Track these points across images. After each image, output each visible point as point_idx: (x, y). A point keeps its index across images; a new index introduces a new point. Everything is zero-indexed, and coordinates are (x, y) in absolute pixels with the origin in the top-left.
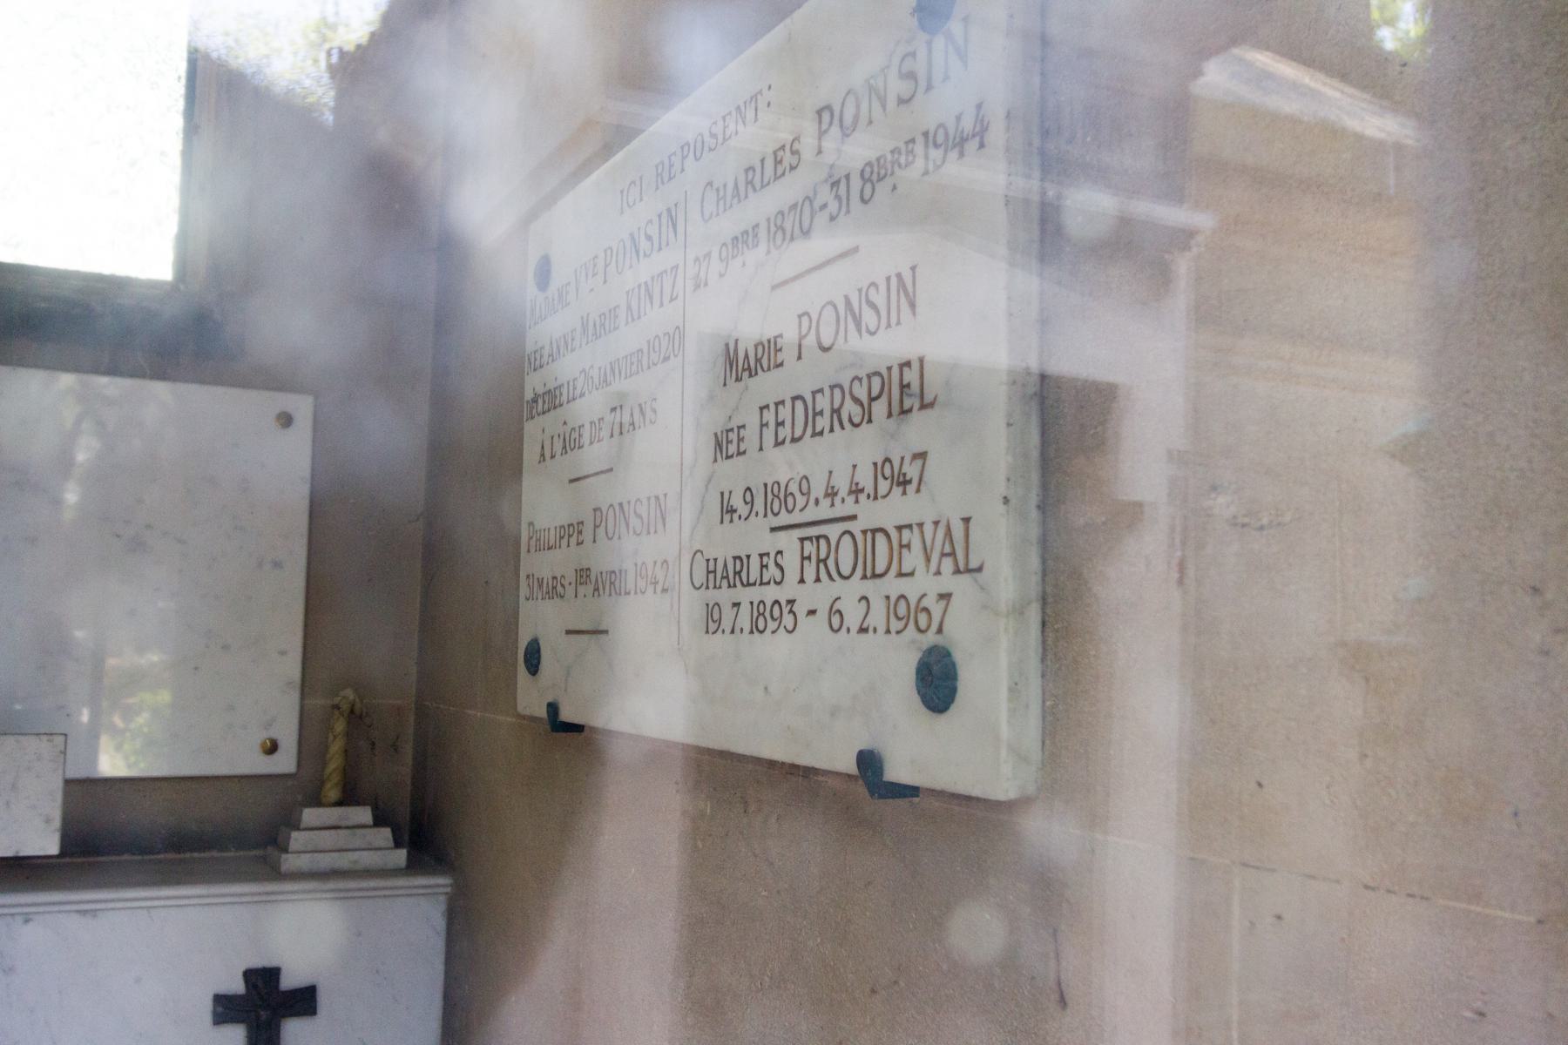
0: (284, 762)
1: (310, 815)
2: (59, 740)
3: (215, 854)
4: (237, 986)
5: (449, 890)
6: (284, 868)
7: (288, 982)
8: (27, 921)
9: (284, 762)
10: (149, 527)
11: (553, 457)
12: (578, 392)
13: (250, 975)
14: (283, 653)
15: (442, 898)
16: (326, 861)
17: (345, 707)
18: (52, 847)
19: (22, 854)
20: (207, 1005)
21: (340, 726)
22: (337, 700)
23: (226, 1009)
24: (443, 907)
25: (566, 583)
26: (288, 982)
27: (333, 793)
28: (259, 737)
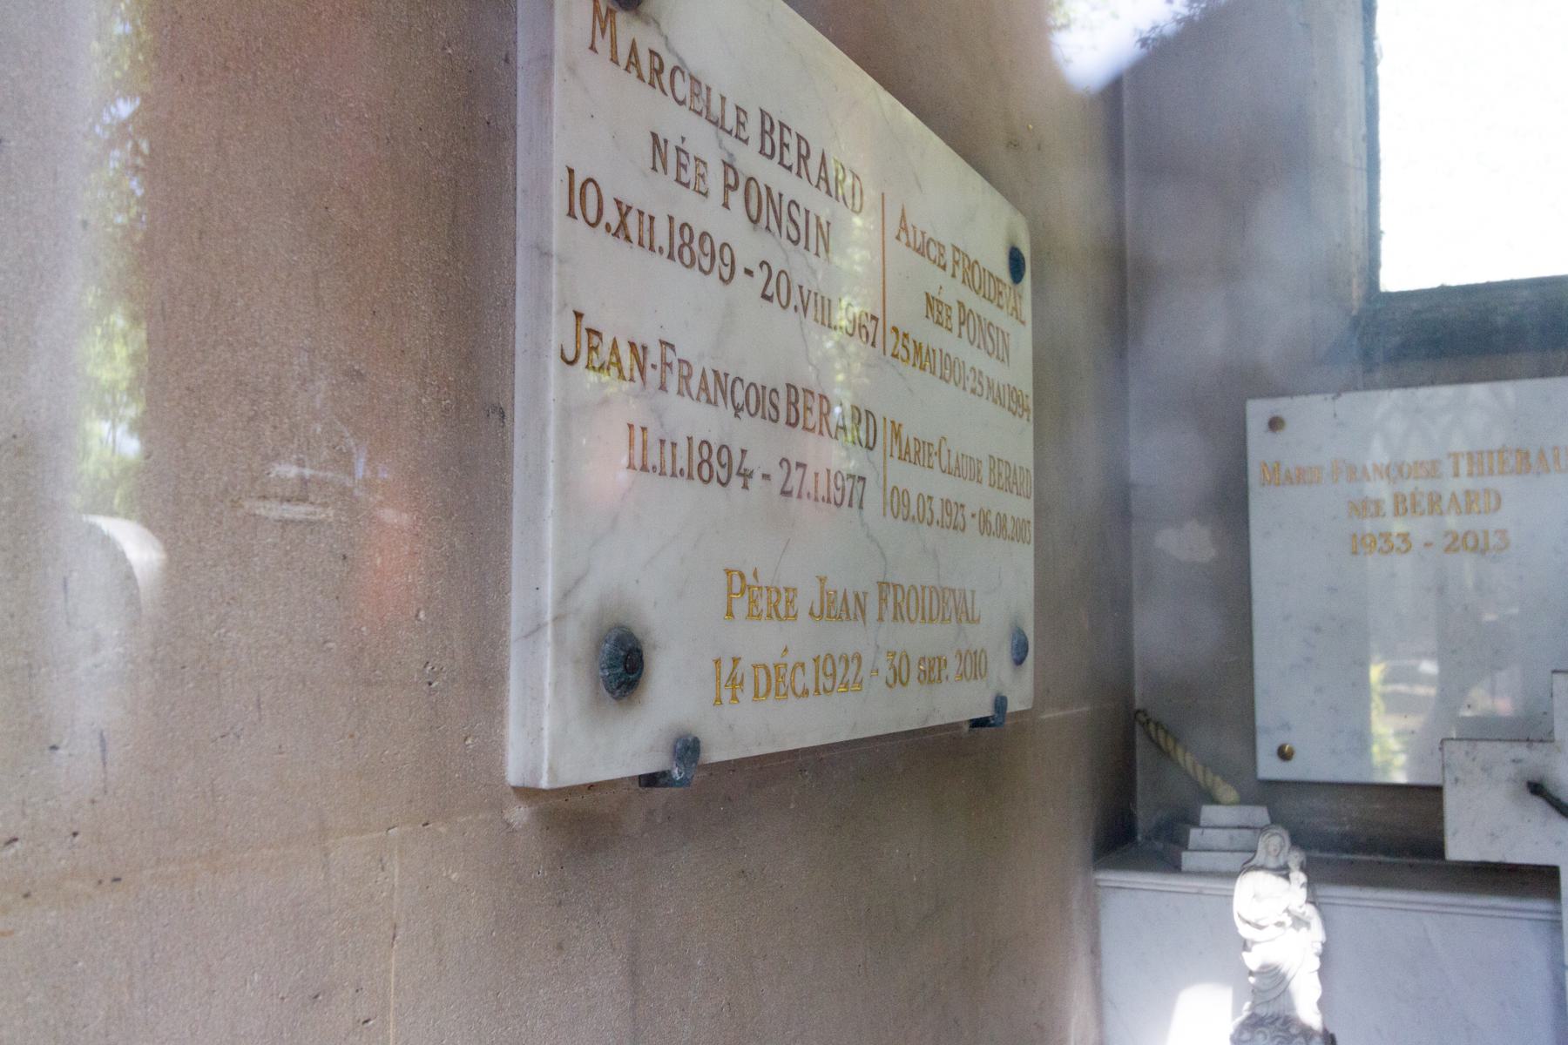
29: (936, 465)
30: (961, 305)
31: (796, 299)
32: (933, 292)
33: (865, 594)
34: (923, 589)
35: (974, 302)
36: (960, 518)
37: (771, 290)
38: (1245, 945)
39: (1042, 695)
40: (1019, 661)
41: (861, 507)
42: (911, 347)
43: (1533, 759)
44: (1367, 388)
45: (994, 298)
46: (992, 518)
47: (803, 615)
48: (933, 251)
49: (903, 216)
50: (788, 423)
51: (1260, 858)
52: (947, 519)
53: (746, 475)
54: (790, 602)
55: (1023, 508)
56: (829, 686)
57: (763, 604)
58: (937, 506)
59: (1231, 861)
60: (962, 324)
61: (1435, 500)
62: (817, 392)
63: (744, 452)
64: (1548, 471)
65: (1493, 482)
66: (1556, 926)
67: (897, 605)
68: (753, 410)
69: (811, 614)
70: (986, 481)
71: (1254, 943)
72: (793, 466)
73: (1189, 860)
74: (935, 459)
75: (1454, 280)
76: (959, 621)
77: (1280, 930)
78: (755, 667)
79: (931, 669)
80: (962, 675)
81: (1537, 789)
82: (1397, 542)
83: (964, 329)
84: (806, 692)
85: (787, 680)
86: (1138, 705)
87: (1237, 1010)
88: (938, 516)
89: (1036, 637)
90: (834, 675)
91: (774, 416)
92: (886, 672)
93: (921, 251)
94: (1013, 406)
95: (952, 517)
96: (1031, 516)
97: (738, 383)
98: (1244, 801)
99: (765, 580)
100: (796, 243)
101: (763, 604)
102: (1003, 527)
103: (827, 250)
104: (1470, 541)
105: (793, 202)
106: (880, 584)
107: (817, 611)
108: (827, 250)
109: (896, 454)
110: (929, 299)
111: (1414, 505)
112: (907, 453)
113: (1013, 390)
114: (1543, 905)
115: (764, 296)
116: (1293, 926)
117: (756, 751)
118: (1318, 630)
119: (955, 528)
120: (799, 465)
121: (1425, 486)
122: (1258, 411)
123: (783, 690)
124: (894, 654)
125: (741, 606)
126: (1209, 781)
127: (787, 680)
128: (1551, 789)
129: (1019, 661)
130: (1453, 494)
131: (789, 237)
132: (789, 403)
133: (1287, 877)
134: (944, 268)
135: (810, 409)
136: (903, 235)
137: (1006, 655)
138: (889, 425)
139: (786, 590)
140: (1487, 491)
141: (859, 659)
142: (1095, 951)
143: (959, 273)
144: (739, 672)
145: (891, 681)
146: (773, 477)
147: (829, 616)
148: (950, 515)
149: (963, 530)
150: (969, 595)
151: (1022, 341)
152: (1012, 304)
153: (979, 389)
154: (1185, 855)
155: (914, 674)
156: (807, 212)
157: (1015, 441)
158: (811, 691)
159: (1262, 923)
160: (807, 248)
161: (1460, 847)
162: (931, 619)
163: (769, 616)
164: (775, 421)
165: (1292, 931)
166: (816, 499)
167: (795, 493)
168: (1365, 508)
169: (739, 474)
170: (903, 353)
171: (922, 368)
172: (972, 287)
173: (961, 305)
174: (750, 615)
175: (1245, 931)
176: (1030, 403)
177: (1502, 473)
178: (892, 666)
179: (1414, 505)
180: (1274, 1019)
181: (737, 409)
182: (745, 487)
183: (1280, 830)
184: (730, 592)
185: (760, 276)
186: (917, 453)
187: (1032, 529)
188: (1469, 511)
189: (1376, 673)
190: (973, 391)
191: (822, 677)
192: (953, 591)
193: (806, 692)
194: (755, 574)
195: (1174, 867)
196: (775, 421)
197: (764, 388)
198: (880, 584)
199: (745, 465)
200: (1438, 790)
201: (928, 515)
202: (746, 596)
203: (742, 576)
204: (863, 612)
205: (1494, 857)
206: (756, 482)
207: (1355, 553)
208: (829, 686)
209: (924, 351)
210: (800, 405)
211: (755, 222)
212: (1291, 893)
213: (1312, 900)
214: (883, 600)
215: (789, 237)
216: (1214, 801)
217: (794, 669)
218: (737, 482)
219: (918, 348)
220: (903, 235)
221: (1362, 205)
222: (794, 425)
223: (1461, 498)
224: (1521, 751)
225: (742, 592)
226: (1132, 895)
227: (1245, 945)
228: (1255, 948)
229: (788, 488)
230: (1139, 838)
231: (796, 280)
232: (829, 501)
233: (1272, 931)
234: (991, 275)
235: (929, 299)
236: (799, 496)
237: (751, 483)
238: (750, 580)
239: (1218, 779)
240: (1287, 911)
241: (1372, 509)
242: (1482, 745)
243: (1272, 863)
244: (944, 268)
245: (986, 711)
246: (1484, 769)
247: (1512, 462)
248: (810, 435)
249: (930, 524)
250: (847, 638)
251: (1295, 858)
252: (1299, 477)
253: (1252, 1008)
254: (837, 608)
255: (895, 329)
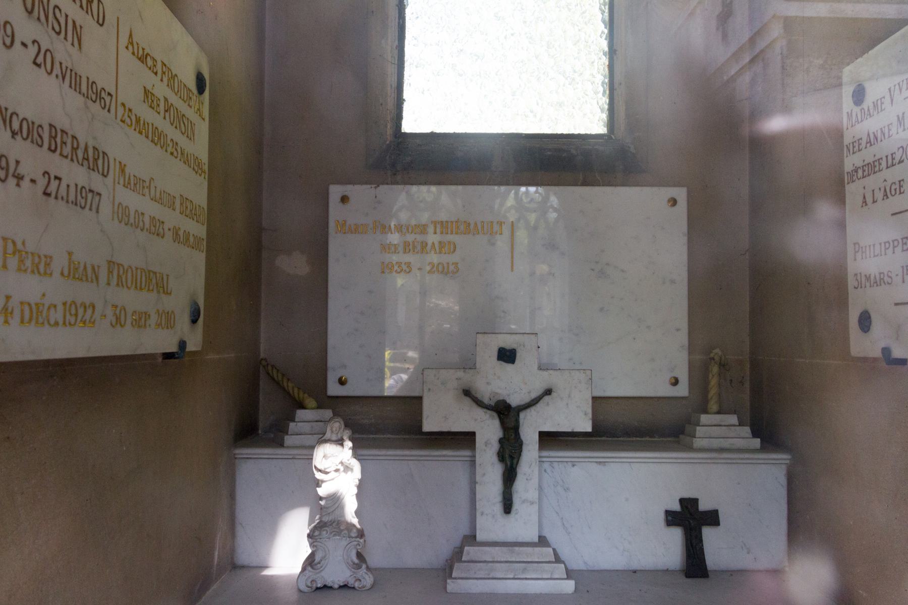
0: (682, 390)
1: (704, 418)
2: (588, 372)
3: (647, 439)
4: (677, 507)
5: (788, 462)
6: (695, 446)
7: (703, 506)
8: (573, 466)
9: (682, 390)
10: (607, 264)
11: (874, 202)
12: (897, 160)
13: (682, 501)
14: (678, 330)
15: (784, 467)
16: (716, 443)
17: (717, 358)
18: (589, 429)
19: (575, 430)
20: (662, 516)
21: (715, 369)
22: (712, 355)
23: (672, 519)
24: (784, 472)
25: (893, 275)
26: (703, 506)
27: (713, 406)
28: (668, 377)
29: (147, 194)
30: (166, 99)
31: (57, 70)
32: (149, 87)
33: (99, 267)
34: (137, 269)
35: (174, 100)
36: (161, 230)
37: (40, 60)
38: (318, 483)
39: (208, 342)
40: (194, 321)
41: (97, 212)
42: (133, 118)
43: (466, 377)
44: (393, 183)
45: (187, 100)
46: (181, 233)
47: (56, 274)
48: (150, 62)
49: (131, 35)
50: (50, 149)
51: (328, 435)
52: (153, 229)
53: (19, 178)
54: (47, 265)
55: (199, 230)
56: (73, 321)
57: (28, 263)
58: (147, 220)
59: (309, 440)
60: (166, 111)
61: (424, 245)
62: (70, 133)
63: (18, 162)
64: (478, 233)
65: (450, 237)
66: (473, 463)
67: (119, 276)
68: (25, 135)
69: (62, 274)
70: (178, 211)
71: (323, 481)
72: (52, 177)
73: (289, 440)
74: (146, 190)
75: (438, 130)
76: (158, 292)
77: (337, 474)
78: (22, 303)
79: (140, 319)
80: (159, 325)
81: (467, 393)
82: (404, 267)
83: (167, 115)
84: (57, 324)
85: (44, 315)
86: (262, 355)
87: (311, 520)
88: (147, 226)
89: (205, 306)
90: (76, 315)
91: (40, 143)
92: (110, 317)
93: (143, 59)
94: (196, 168)
95: (156, 228)
96: (204, 237)
97: (14, 117)
98: (320, 407)
99: (30, 247)
100: (59, 33)
101: (28, 263)
102: (188, 239)
103: (80, 44)
104: (440, 269)
105: (56, 7)
106: (109, 262)
107: (66, 273)
108: (80, 44)
109: (122, 182)
110: (146, 92)
111: (414, 247)
112: (129, 183)
113: (184, 200)
114: (467, 453)
115: (35, 63)
116: (344, 471)
117: (20, 358)
118: (362, 313)
119: (158, 235)
120: (56, 178)
121: (419, 238)
122: (336, 191)
123: (41, 320)
124: (116, 307)
125: (13, 262)
126: (301, 395)
127: (44, 315)
128: (473, 393)
129: (194, 321)
130: (433, 243)
131: (53, 28)
132: (51, 136)
133: (342, 445)
134: (156, 74)
135: (65, 143)
136: (130, 47)
137: (186, 318)
138: (118, 164)
139: (46, 256)
140: (449, 242)
141: (94, 307)
142: (232, 496)
143: (165, 79)
144: (10, 305)
145: (114, 323)
146: (38, 182)
147: (74, 277)
148: (155, 226)
149: (163, 237)
150: (165, 278)
151: (203, 129)
152: (197, 107)
153: (175, 153)
154: (286, 437)
155: (129, 321)
156: (67, 16)
157: (197, 191)
158: (61, 322)
159: (327, 470)
160: (66, 38)
161: (429, 426)
162: (141, 289)
163: (33, 272)
164: (41, 146)
165: (343, 474)
166: (67, 202)
167: (53, 195)
168: (389, 248)
169: (14, 176)
170: (128, 120)
171: (140, 133)
172: (173, 89)
173: (166, 99)
174: (19, 269)
175: (318, 476)
176: (206, 168)
177: (456, 233)
178: (115, 314)
179: (414, 247)
180: (332, 523)
181: (14, 134)
182: (18, 185)
183: (339, 419)
184: (5, 253)
185: (33, 50)
186: (135, 184)
187: (205, 243)
188: (440, 253)
189: (387, 354)
190: (172, 154)
191: (68, 314)
192: (155, 273)
193: (57, 324)
194: (24, 243)
195: (281, 445)
196: (41, 146)
197: (33, 123)
198: (109, 262)
199: (18, 172)
200: (420, 399)
201: (141, 224)
202: (17, 256)
203: (14, 243)
204: (97, 279)
205: (445, 429)
206: (26, 183)
207: (383, 272)
208: (73, 321)
209: (142, 122)
210: (58, 140)
211: (30, 12)
212: (345, 453)
213: (356, 455)
214: (110, 272)
215: (53, 28)
216: (302, 406)
217: (49, 308)
218: (12, 181)
219: (138, 120)
220: (130, 47)
221: (395, 85)
222: (54, 151)
223: (437, 246)
224: (460, 374)
225: (14, 253)
226: (256, 468)
227: (318, 483)
228: (324, 485)
229: (48, 191)
230: (260, 432)
231: (58, 57)
232: (76, 204)
233: (333, 475)
234: (185, 85)
235: (146, 92)
236: (56, 198)
237: (22, 183)
238: (19, 246)
239: (306, 395)
240: (342, 463)
241: (393, 249)
242: (443, 372)
243: (334, 438)
244: (156, 74)
245: (173, 349)
246: (443, 384)
247: (462, 227)
248: (64, 160)
249: (142, 230)
250: (84, 292)
251: (347, 434)
252: (356, 230)
253: (320, 518)
254: (77, 273)
255: (123, 105)
